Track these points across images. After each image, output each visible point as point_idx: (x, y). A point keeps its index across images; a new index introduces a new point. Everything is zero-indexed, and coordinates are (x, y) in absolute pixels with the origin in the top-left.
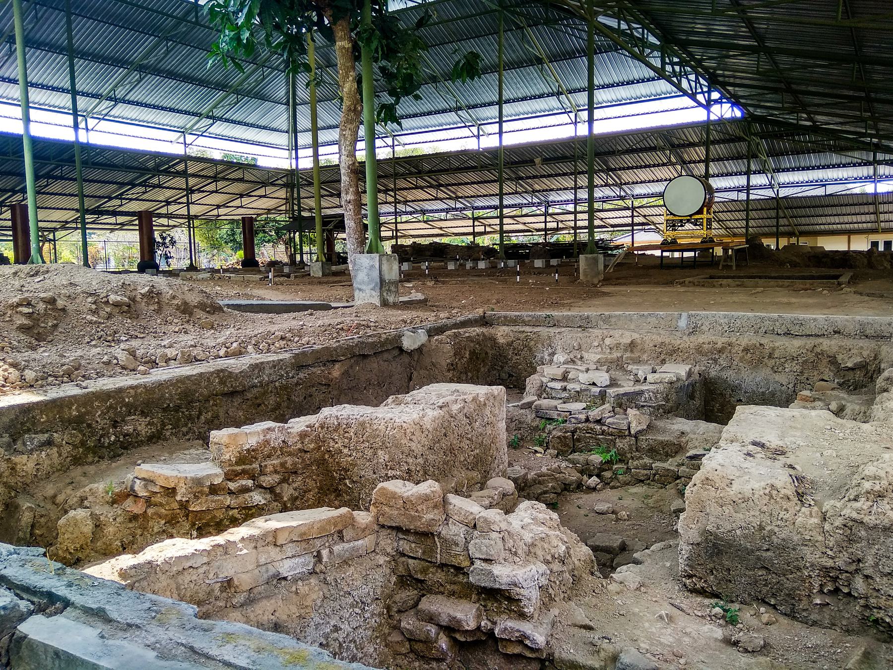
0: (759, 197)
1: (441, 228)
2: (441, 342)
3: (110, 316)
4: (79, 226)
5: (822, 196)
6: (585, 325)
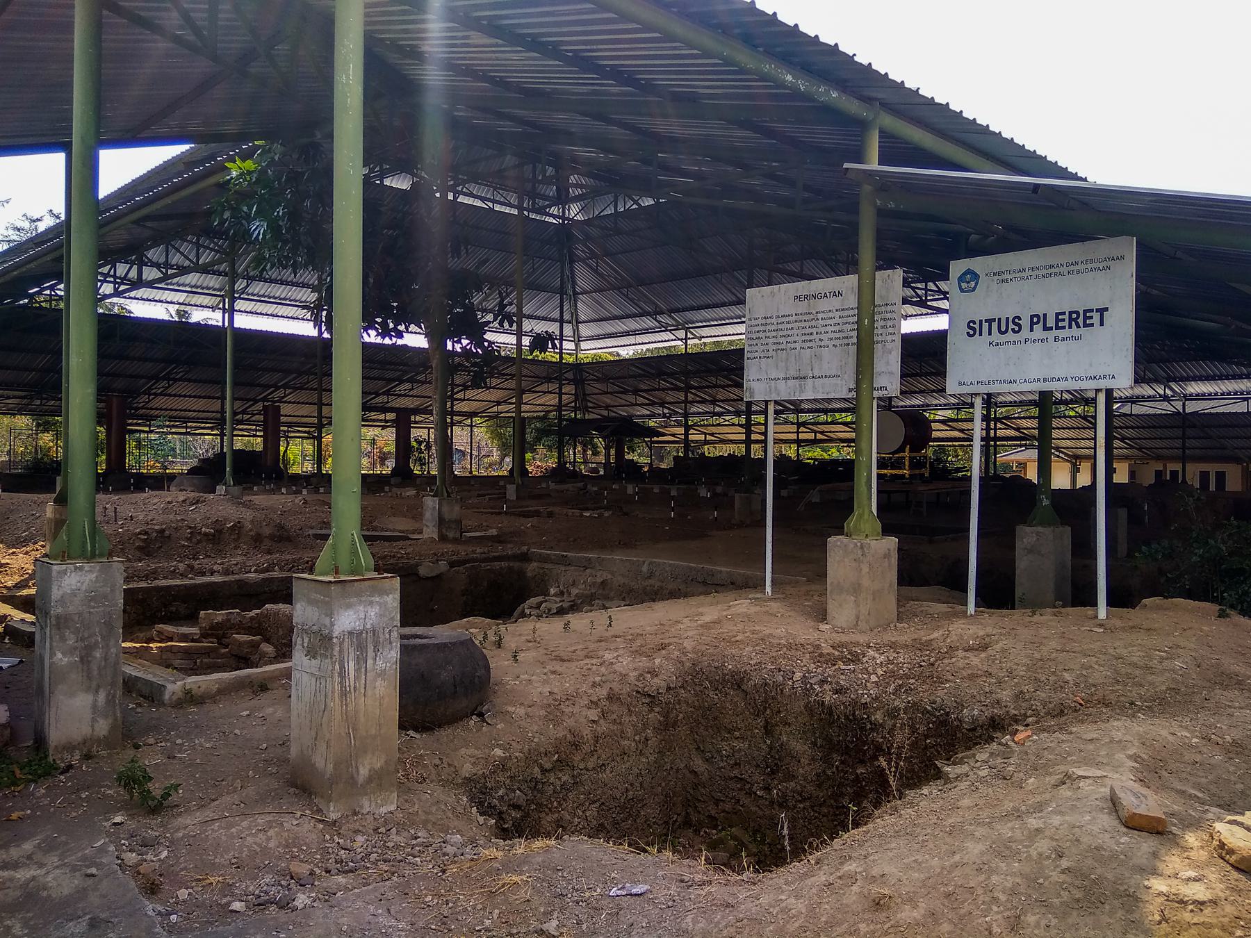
0: (1159, 412)
2: (458, 572)
3: (199, 542)
6: (587, 565)
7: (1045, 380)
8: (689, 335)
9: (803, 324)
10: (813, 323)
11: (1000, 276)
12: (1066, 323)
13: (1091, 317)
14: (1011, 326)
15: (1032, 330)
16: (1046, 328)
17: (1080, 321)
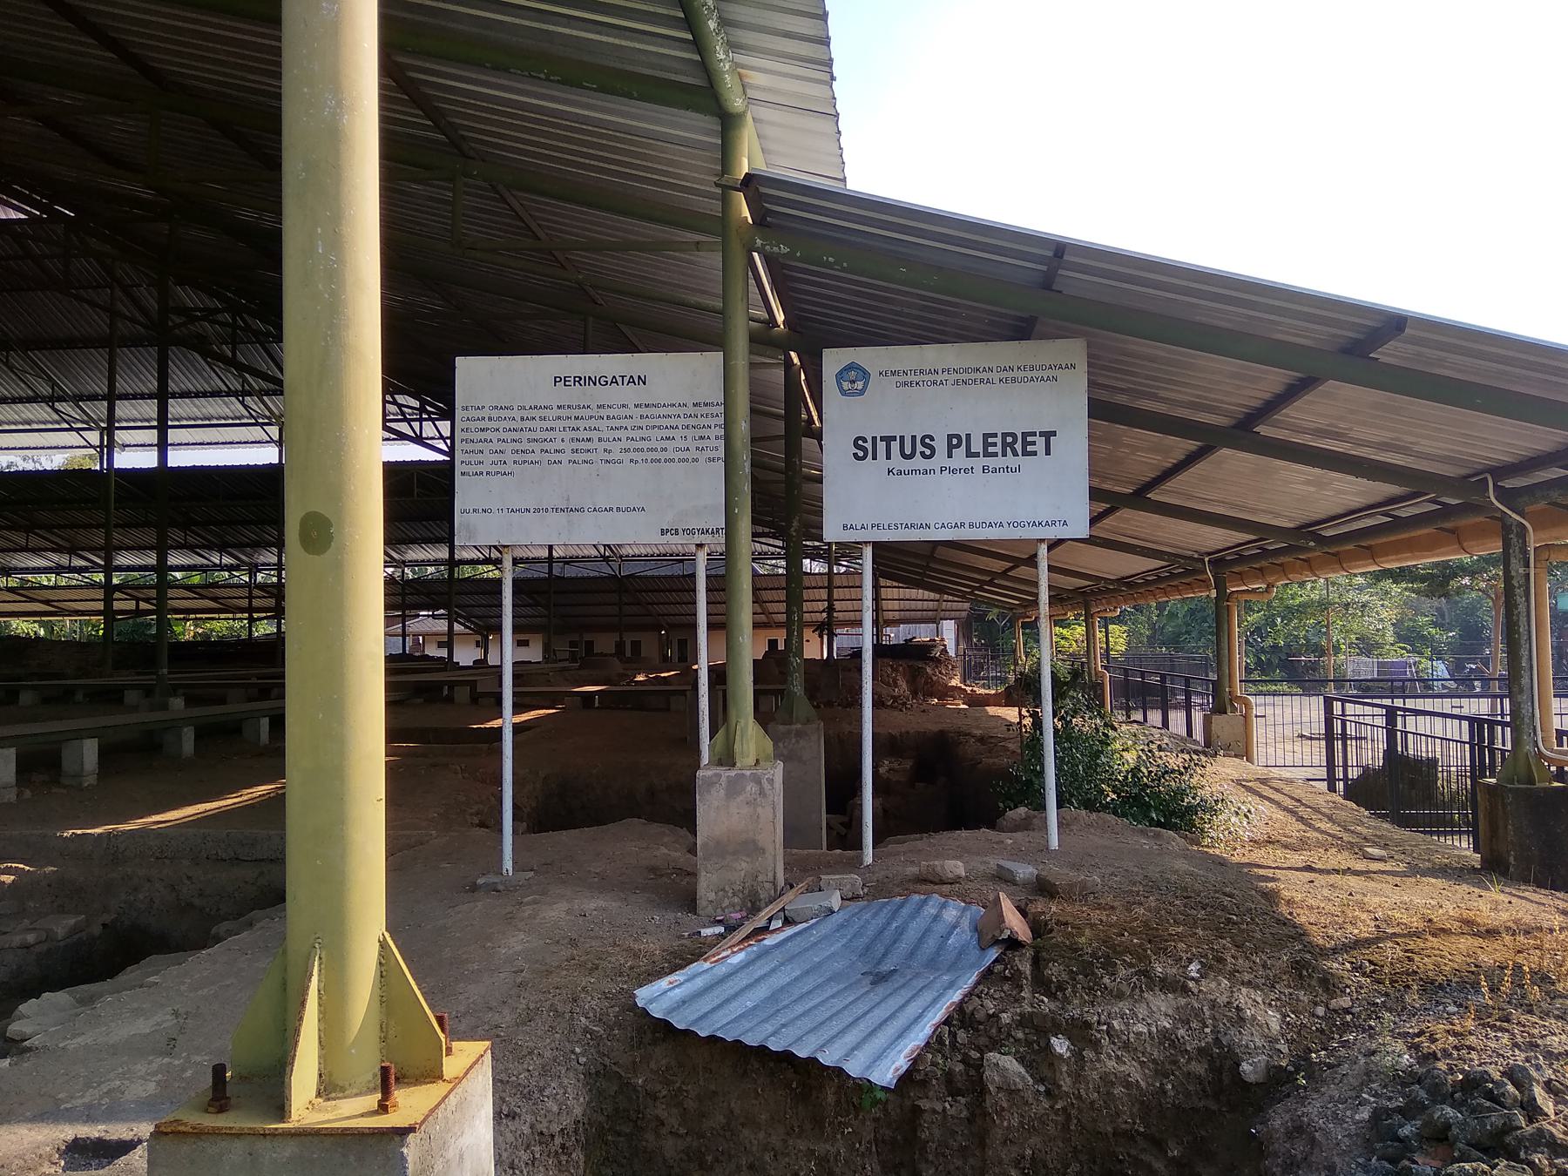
5: (678, 577)
9: (573, 423)
10: (593, 423)
11: (907, 380)
12: (998, 449)
13: (1034, 443)
14: (920, 448)
15: (950, 456)
16: (970, 454)
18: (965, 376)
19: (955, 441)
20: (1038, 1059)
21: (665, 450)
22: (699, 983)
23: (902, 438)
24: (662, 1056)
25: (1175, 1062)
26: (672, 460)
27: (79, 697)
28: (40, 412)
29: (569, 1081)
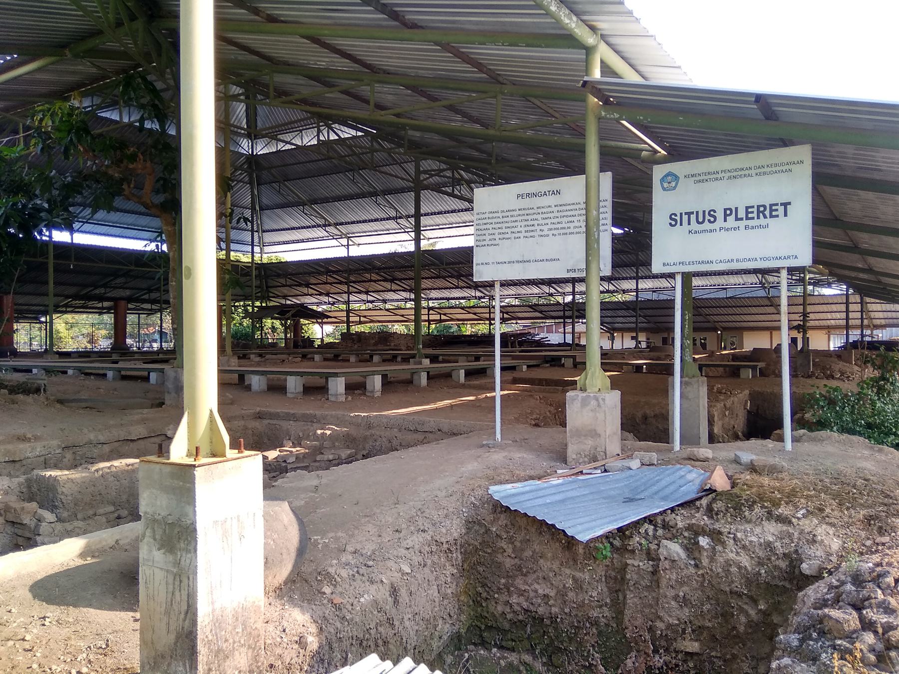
1: (402, 316)
4: (413, 296)
5: (723, 299)
7: (737, 261)
8: (350, 243)
9: (526, 217)
10: (535, 217)
11: (700, 179)
12: (755, 215)
13: (777, 210)
14: (707, 217)
15: (725, 220)
16: (737, 219)
17: (767, 213)
18: (735, 174)
19: (728, 212)
20: (692, 548)
21: (569, 228)
22: (527, 488)
23: (697, 212)
24: (503, 520)
25: (769, 559)
26: (573, 233)
27: (399, 359)
28: (392, 224)
29: (456, 521)
